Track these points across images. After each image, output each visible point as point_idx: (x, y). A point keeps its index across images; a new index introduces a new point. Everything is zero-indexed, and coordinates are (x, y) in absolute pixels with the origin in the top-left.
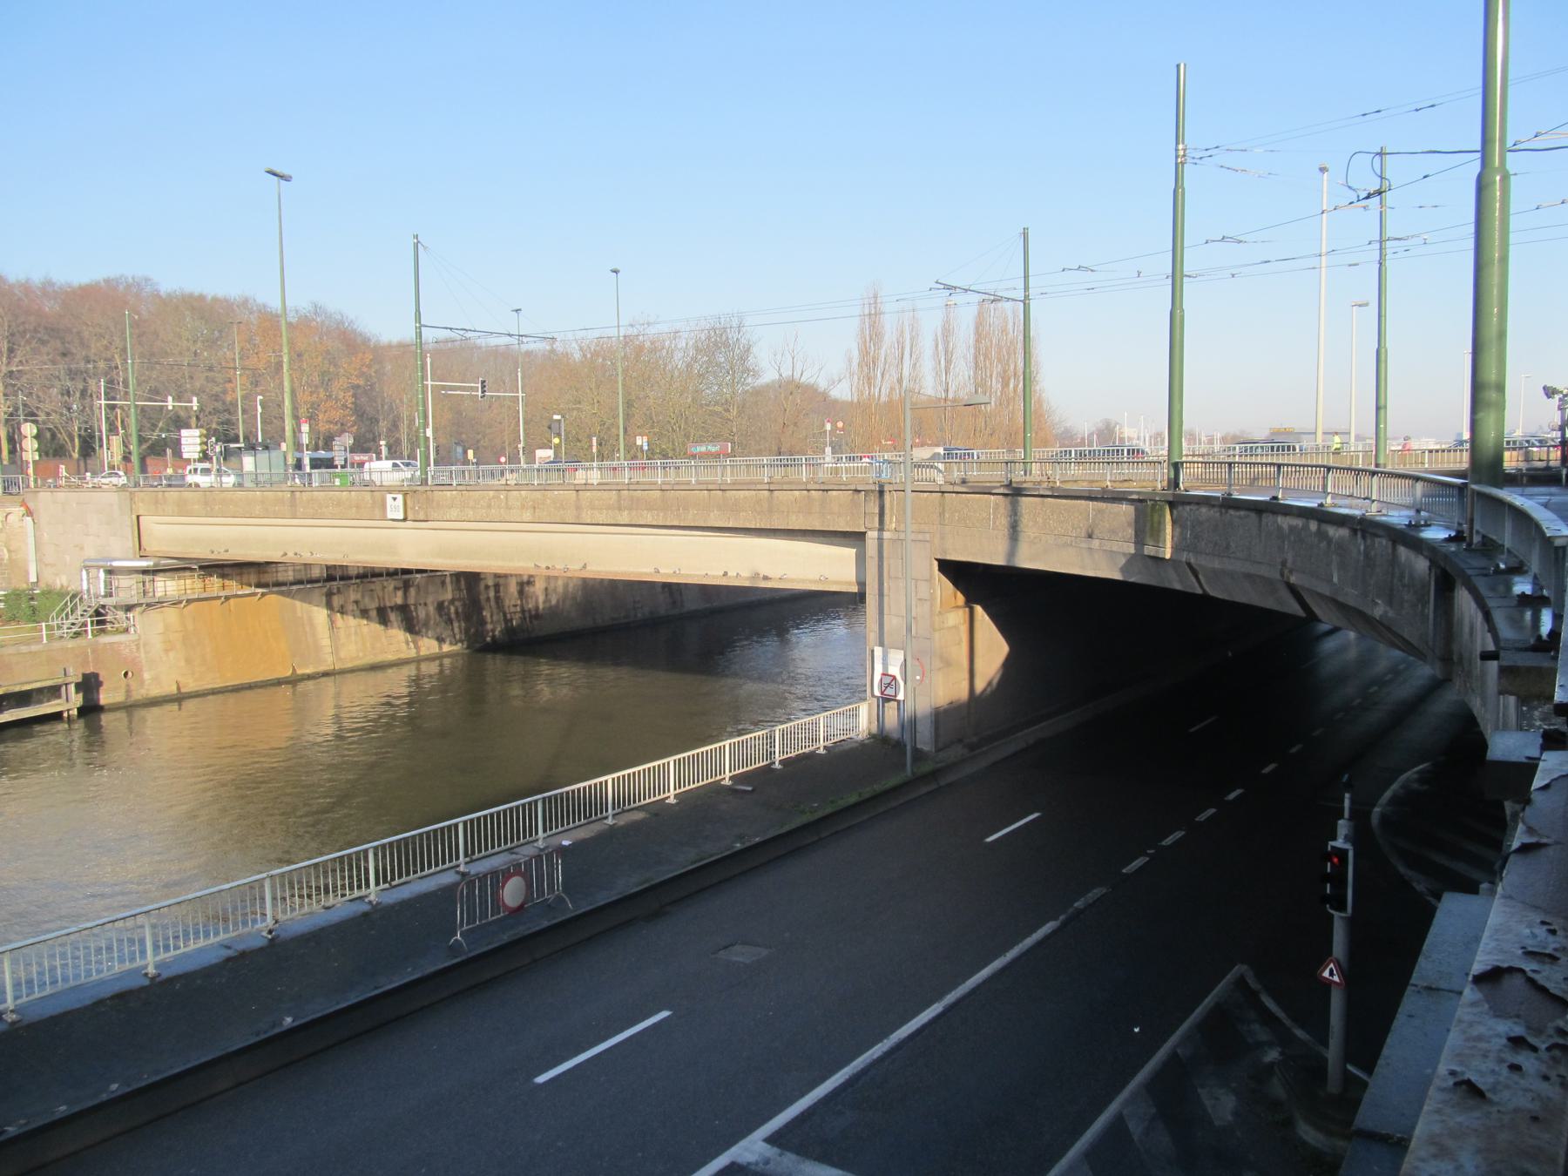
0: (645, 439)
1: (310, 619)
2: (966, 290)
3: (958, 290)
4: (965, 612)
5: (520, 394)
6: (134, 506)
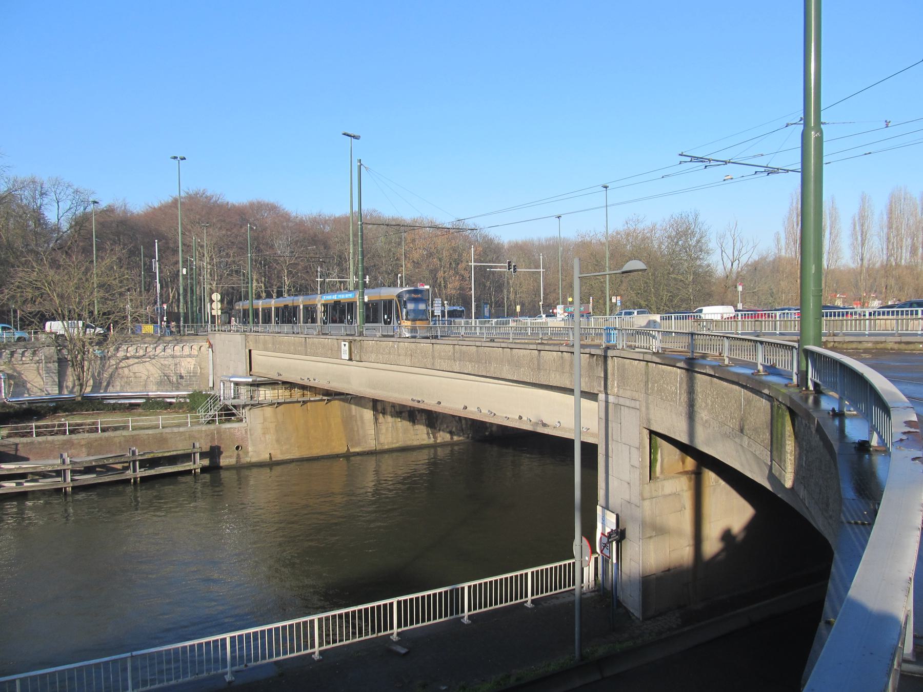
0: (619, 298)
1: (362, 417)
2: (726, 163)
3: (713, 163)
4: (686, 478)
5: (542, 270)
6: (247, 344)
